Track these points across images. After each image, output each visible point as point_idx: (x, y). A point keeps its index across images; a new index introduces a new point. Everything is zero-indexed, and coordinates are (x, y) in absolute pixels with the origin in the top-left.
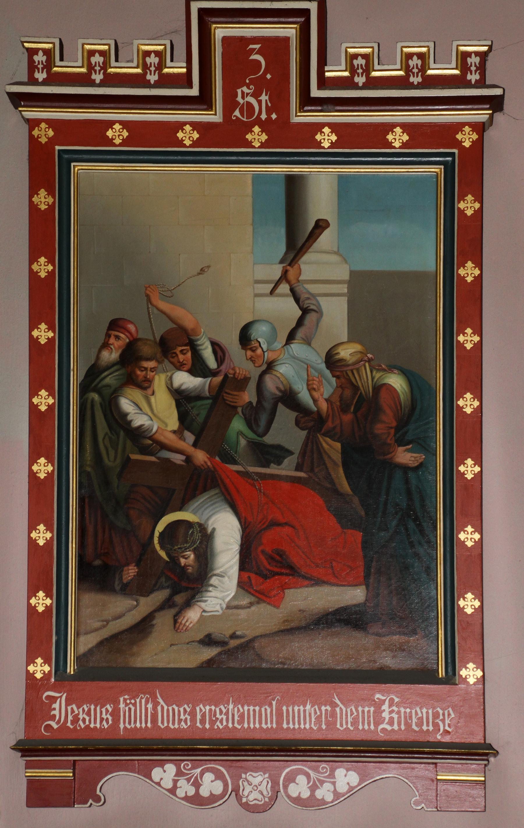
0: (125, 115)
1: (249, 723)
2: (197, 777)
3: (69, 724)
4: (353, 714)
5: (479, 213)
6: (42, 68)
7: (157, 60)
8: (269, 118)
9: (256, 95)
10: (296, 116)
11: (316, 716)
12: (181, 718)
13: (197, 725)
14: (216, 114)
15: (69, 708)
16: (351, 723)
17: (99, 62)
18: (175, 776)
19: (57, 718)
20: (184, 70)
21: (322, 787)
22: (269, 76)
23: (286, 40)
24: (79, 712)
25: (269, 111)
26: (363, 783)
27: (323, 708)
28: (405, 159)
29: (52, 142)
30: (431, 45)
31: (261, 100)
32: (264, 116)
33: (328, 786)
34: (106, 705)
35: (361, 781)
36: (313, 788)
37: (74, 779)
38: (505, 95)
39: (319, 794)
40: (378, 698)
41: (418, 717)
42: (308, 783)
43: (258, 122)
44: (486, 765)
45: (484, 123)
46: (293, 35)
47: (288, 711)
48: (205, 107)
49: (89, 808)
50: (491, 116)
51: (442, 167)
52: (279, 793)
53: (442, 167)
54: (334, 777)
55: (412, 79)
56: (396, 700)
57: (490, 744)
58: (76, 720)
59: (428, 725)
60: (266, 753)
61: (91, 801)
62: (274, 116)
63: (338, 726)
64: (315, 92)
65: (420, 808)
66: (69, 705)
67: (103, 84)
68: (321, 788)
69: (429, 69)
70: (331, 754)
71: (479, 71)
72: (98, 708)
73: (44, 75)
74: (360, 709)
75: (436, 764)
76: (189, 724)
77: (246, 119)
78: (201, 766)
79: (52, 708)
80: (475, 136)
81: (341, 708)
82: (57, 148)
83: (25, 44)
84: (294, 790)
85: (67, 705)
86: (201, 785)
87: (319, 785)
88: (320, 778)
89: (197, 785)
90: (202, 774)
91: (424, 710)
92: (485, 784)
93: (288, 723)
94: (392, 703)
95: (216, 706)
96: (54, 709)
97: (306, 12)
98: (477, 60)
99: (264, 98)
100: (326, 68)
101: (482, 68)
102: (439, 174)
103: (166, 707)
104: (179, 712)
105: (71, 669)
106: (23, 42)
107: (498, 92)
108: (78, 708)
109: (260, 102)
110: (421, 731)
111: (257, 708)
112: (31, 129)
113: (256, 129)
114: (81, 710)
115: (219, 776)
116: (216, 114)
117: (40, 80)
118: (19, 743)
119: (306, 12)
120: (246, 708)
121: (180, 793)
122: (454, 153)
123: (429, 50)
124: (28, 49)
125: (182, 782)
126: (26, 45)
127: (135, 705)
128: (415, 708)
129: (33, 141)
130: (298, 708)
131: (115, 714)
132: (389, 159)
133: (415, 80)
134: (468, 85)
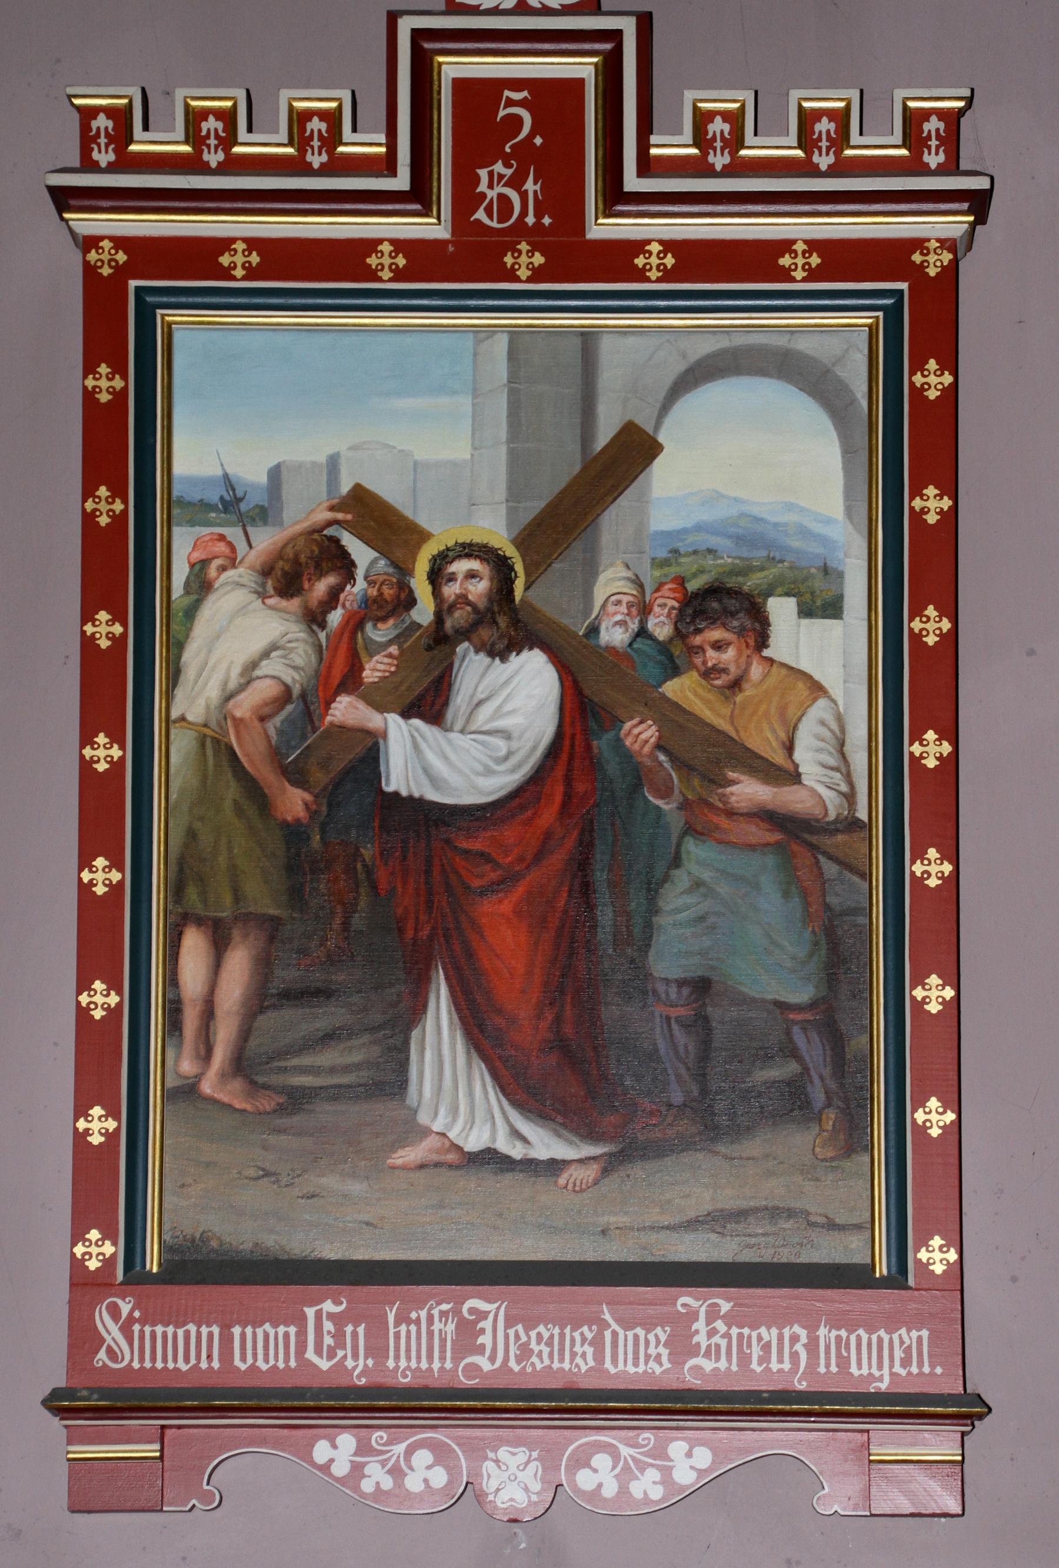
8: (538, 223)
9: (516, 182)
11: (520, 1342)
14: (440, 224)
18: (355, 1454)
19: (488, 1352)
20: (383, 150)
22: (538, 141)
23: (580, 83)
24: (529, 1337)
29: (122, 273)
31: (526, 191)
32: (530, 220)
33: (653, 1475)
34: (581, 1326)
36: (625, 1476)
37: (161, 1457)
39: (636, 1489)
40: (684, 1305)
41: (520, 1342)
42: (614, 1468)
47: (243, 1336)
48: (418, 207)
50: (973, 226)
51: (880, 314)
53: (880, 314)
56: (725, 1307)
57: (979, 1395)
58: (525, 1352)
59: (780, 1361)
61: (194, 1501)
62: (547, 221)
65: (187, 1508)
66: (512, 1327)
72: (568, 1330)
75: (868, 1431)
78: (407, 1439)
79: (693, 1330)
80: (947, 257)
82: (133, 284)
83: (73, 100)
84: (585, 1480)
85: (507, 1327)
86: (406, 1475)
87: (638, 1474)
89: (397, 1473)
90: (409, 1452)
94: (713, 1315)
95: (850, 1332)
96: (697, 1332)
97: (616, 36)
99: (530, 186)
100: (654, 139)
101: (951, 141)
102: (874, 328)
103: (621, 1333)
105: (153, 1266)
106: (70, 97)
107: (981, 183)
109: (524, 196)
111: (170, 1330)
115: (442, 1455)
116: (440, 224)
117: (718, 167)
119: (616, 36)
121: (367, 1486)
122: (901, 292)
124: (79, 109)
126: (77, 102)
127: (418, 1322)
129: (90, 271)
134: (924, 171)
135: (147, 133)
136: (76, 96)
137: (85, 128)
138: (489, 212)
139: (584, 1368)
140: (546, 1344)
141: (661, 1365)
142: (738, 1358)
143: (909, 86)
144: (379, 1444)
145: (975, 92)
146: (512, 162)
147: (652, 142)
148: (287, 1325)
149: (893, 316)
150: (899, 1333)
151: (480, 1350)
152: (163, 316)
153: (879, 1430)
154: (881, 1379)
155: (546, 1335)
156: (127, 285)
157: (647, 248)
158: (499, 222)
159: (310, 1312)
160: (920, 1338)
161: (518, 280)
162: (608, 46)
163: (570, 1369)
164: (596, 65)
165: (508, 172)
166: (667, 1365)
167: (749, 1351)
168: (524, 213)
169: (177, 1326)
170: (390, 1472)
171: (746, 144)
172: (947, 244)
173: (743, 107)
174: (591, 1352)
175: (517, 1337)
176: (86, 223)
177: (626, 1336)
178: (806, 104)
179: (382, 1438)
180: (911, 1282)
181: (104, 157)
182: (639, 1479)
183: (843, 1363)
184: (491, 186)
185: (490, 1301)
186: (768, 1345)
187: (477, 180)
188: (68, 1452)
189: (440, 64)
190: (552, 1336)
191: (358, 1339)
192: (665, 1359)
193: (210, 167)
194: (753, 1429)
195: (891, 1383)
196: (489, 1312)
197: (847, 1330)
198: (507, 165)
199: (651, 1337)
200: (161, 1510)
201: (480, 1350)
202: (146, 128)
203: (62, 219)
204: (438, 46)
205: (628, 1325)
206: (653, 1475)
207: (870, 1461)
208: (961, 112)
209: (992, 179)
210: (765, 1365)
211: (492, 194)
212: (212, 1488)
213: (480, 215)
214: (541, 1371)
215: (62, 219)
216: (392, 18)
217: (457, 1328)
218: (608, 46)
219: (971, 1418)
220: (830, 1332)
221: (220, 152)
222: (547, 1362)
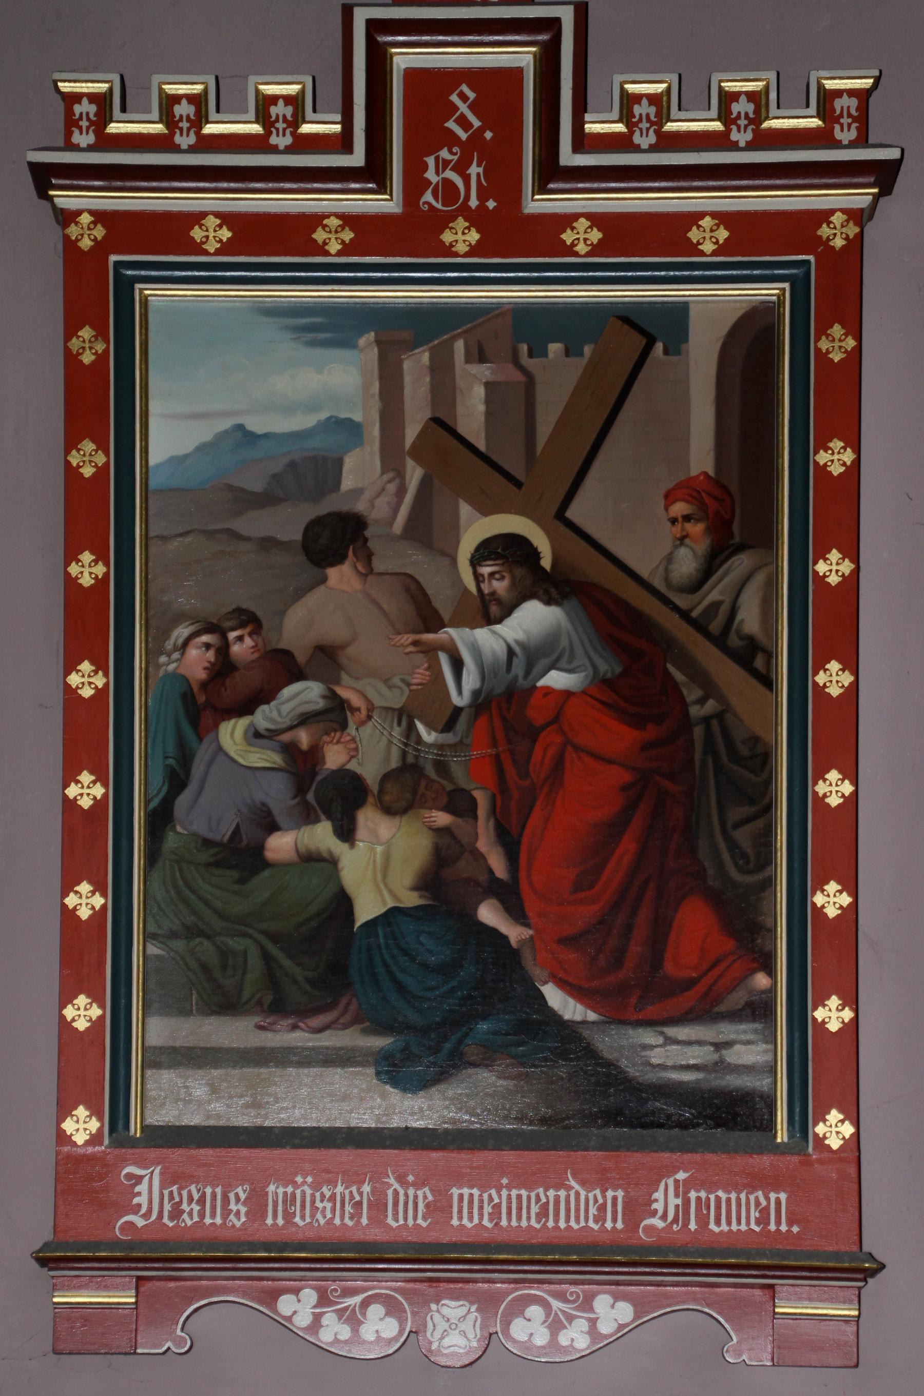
0: (161, 201)
1: (556, 1220)
2: (354, 1310)
3: (166, 1220)
4: (761, 1204)
6: (843, 117)
8: (482, 206)
9: (461, 168)
10: (533, 200)
11: (761, 1207)
15: (166, 1192)
16: (537, 1215)
19: (660, 1213)
20: (338, 128)
21: (342, 1323)
22: (488, 135)
23: (517, 73)
25: (483, 196)
26: (575, 1315)
28: (585, 274)
29: (101, 248)
31: (469, 175)
32: (474, 203)
35: (637, 1317)
36: (555, 1326)
37: (136, 1308)
41: (761, 1207)
43: (465, 211)
45: (862, 210)
46: (528, 64)
49: (856, 1370)
50: (876, 198)
51: (786, 286)
53: (786, 286)
54: (591, 1310)
55: (273, 140)
57: (870, 1254)
58: (176, 1213)
60: (358, 1266)
62: (491, 204)
63: (390, 1221)
64: (568, 157)
66: (165, 1189)
67: (751, 146)
68: (568, 1326)
69: (304, 122)
71: (93, 127)
73: (749, 136)
74: (773, 1196)
75: (772, 1287)
76: (243, 1219)
77: (443, 205)
80: (852, 230)
82: (113, 258)
83: (59, 84)
84: (519, 1330)
85: (162, 1187)
87: (344, 1318)
88: (564, 1309)
90: (365, 1304)
91: (610, 1194)
92: (858, 1321)
96: (656, 1200)
97: (554, 24)
98: (853, 103)
99: (474, 170)
100: (588, 117)
101: (863, 119)
107: (893, 154)
110: (603, 1229)
113: (461, 223)
114: (185, 1193)
116: (391, 200)
118: (46, 1246)
119: (554, 24)
120: (504, 1193)
122: (808, 262)
125: (329, 1317)
128: (187, 1187)
131: (378, 1206)
132: (512, 275)
135: (124, 114)
136: (64, 81)
137: (69, 112)
138: (435, 195)
140: (329, 1200)
142: (697, 1216)
143: (726, 70)
145: (883, 72)
147: (586, 119)
150: (595, 1192)
151: (655, 1212)
152: (141, 290)
155: (328, 1194)
157: (325, 222)
160: (615, 1199)
164: (535, 54)
166: (243, 1219)
168: (468, 197)
169: (530, 1189)
172: (858, 216)
175: (491, 1199)
176: (66, 199)
179: (336, 1290)
181: (84, 139)
185: (147, 1168)
186: (498, 1206)
187: (426, 167)
197: (479, 1189)
200: (135, 1353)
202: (124, 109)
204: (390, 38)
206: (581, 1324)
214: (191, 1226)
216: (347, 13)
220: (277, 1188)
221: (192, 133)
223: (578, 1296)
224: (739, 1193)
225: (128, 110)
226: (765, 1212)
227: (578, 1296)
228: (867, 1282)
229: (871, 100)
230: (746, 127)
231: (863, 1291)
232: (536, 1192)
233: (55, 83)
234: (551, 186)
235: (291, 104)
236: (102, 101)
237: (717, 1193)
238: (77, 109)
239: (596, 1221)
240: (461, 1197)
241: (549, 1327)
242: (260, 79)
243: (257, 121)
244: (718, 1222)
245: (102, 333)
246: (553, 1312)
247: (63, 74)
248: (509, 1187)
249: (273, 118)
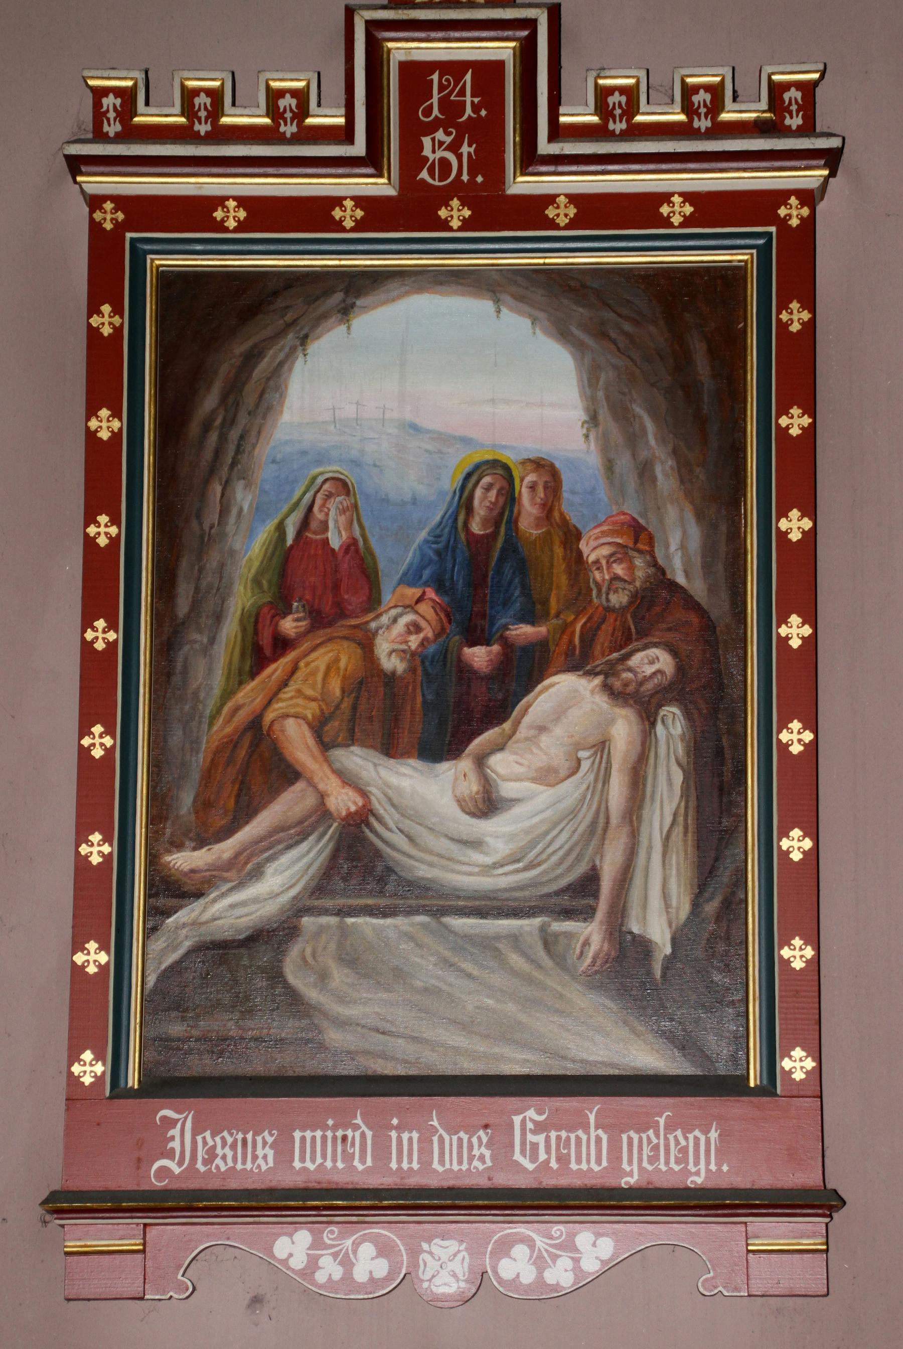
2: (347, 1253)
5: (810, 327)
6: (291, 118)
7: (623, 99)
9: (454, 147)
10: (514, 182)
11: (679, 1147)
12: (473, 1153)
13: (433, 1166)
17: (290, 105)
20: (341, 121)
23: (499, 65)
27: (691, 1137)
29: (120, 228)
30: (642, 74)
31: (461, 154)
32: (465, 177)
36: (540, 1263)
38: (845, 150)
39: (550, 1276)
44: (827, 1224)
50: (826, 179)
51: (754, 251)
52: (484, 1275)
53: (754, 251)
57: (835, 1191)
62: (480, 179)
66: (259, 1135)
68: (552, 1266)
70: (725, 1212)
75: (745, 1223)
79: (168, 1135)
80: (805, 212)
81: (441, 1137)
82: (129, 235)
84: (507, 1269)
89: (347, 1263)
90: (356, 1245)
93: (400, 1160)
97: (531, 24)
99: (465, 149)
100: (562, 110)
101: (809, 106)
103: (447, 1138)
104: (470, 1142)
107: (834, 143)
108: (213, 1136)
109: (459, 157)
112: (92, 212)
114: (218, 1139)
115: (384, 1250)
118: (53, 1197)
119: (531, 24)
121: (321, 1277)
122: (771, 233)
123: (638, 83)
126: (91, 83)
129: (95, 228)
130: (409, 1135)
133: (289, 129)
134: (786, 132)
135: (233, 108)
136: (92, 78)
137: (97, 104)
139: (264, 1168)
141: (484, 1162)
144: (330, 1239)
146: (450, 129)
148: (313, 1130)
149: (764, 253)
153: (757, 1224)
154: (631, 1174)
156: (124, 237)
158: (440, 181)
159: (517, 1120)
161: (451, 229)
162: (525, 33)
163: (252, 1168)
164: (514, 48)
165: (448, 140)
167: (565, 1152)
170: (341, 1263)
171: (311, 114)
172: (808, 198)
173: (723, 81)
174: (489, 1155)
177: (451, 1139)
178: (689, 80)
180: (779, 1091)
181: (112, 128)
182: (551, 1267)
183: (563, 1160)
184: (434, 152)
185: (182, 1113)
186: (656, 1148)
187: (421, 147)
188: (66, 1247)
189: (389, 50)
190: (236, 1141)
191: (316, 1148)
192: (488, 1159)
193: (109, 137)
194: (538, 1222)
195: (706, 1178)
196: (178, 1120)
198: (448, 134)
199: (475, 1140)
200: (142, 1299)
201: (170, 1155)
203: (75, 182)
205: (452, 1130)
207: (749, 1251)
208: (815, 84)
209: (844, 139)
210: (683, 1165)
211: (431, 157)
212: (187, 1281)
213: (424, 175)
215: (75, 182)
216: (350, 13)
217: (720, 1135)
218: (525, 33)
219: (831, 1208)
222: (230, 1164)
223: (561, 1235)
224: (245, 1133)
225: (150, 104)
226: (684, 1150)
227: (561, 1235)
228: (832, 1218)
229: (817, 89)
230: (790, 103)
231: (830, 1225)
232: (203, 1135)
233: (85, 79)
234: (530, 169)
235: (119, 97)
236: (215, 95)
237: (570, 1134)
238: (105, 101)
239: (677, 1162)
240: (303, 1139)
241: (534, 1263)
242: (186, 74)
243: (267, 115)
244: (579, 1161)
245: (117, 310)
246: (537, 1249)
247: (705, 69)
248: (335, 1128)
249: (281, 110)
